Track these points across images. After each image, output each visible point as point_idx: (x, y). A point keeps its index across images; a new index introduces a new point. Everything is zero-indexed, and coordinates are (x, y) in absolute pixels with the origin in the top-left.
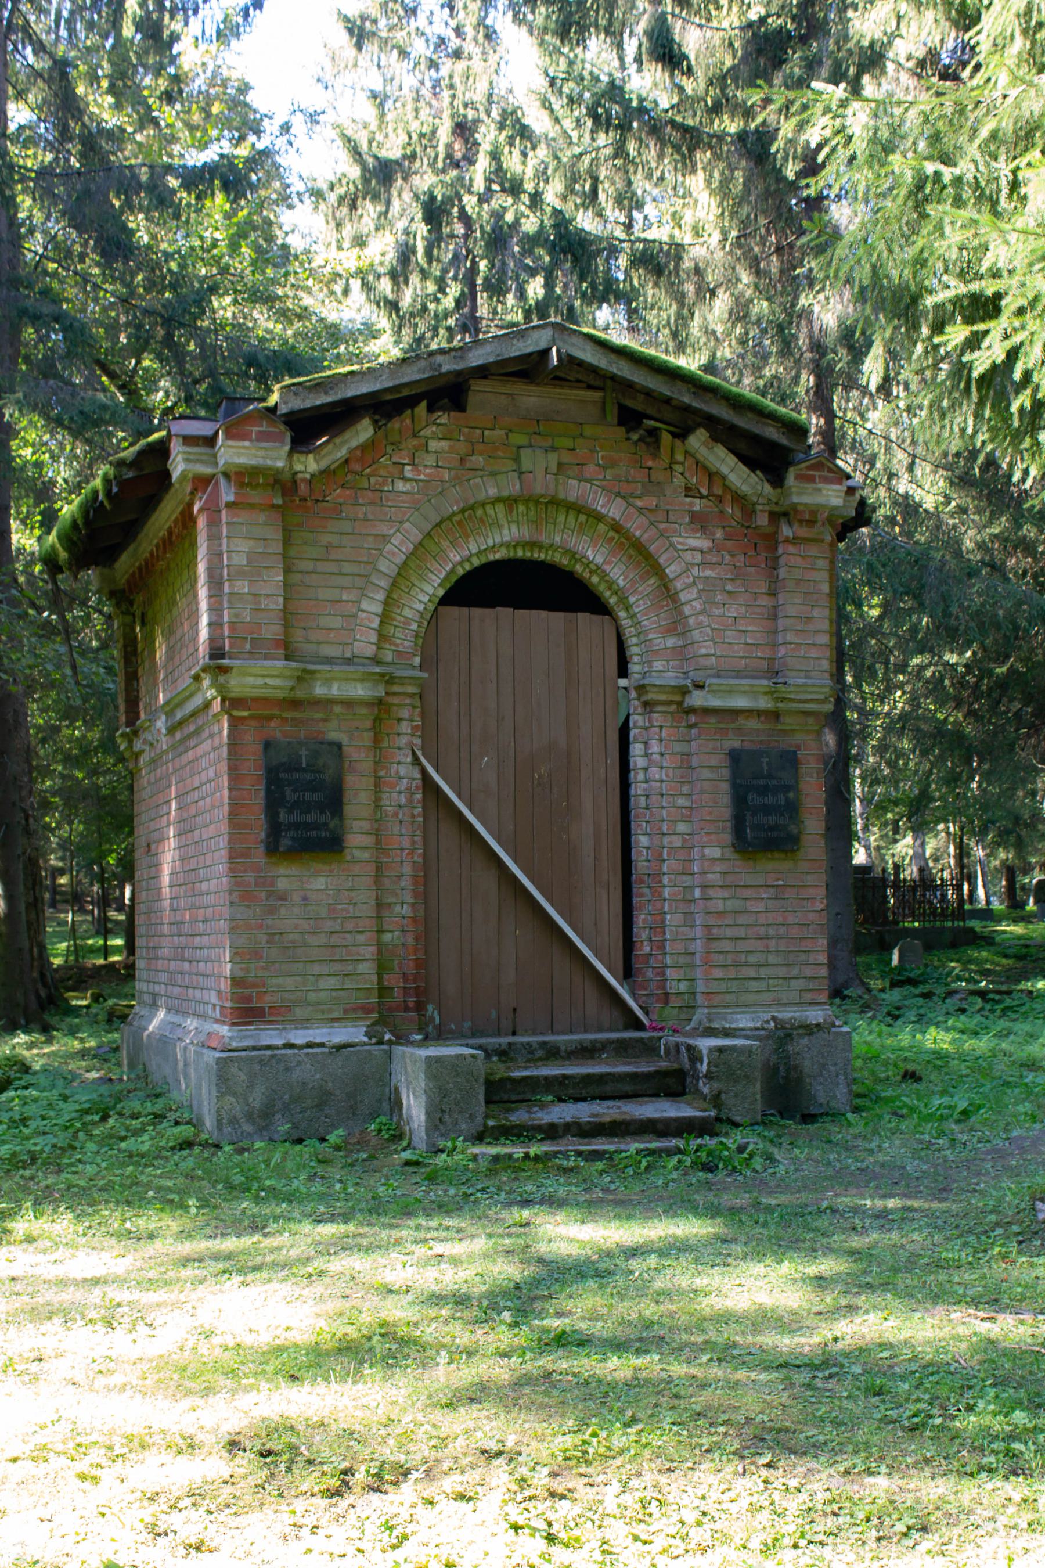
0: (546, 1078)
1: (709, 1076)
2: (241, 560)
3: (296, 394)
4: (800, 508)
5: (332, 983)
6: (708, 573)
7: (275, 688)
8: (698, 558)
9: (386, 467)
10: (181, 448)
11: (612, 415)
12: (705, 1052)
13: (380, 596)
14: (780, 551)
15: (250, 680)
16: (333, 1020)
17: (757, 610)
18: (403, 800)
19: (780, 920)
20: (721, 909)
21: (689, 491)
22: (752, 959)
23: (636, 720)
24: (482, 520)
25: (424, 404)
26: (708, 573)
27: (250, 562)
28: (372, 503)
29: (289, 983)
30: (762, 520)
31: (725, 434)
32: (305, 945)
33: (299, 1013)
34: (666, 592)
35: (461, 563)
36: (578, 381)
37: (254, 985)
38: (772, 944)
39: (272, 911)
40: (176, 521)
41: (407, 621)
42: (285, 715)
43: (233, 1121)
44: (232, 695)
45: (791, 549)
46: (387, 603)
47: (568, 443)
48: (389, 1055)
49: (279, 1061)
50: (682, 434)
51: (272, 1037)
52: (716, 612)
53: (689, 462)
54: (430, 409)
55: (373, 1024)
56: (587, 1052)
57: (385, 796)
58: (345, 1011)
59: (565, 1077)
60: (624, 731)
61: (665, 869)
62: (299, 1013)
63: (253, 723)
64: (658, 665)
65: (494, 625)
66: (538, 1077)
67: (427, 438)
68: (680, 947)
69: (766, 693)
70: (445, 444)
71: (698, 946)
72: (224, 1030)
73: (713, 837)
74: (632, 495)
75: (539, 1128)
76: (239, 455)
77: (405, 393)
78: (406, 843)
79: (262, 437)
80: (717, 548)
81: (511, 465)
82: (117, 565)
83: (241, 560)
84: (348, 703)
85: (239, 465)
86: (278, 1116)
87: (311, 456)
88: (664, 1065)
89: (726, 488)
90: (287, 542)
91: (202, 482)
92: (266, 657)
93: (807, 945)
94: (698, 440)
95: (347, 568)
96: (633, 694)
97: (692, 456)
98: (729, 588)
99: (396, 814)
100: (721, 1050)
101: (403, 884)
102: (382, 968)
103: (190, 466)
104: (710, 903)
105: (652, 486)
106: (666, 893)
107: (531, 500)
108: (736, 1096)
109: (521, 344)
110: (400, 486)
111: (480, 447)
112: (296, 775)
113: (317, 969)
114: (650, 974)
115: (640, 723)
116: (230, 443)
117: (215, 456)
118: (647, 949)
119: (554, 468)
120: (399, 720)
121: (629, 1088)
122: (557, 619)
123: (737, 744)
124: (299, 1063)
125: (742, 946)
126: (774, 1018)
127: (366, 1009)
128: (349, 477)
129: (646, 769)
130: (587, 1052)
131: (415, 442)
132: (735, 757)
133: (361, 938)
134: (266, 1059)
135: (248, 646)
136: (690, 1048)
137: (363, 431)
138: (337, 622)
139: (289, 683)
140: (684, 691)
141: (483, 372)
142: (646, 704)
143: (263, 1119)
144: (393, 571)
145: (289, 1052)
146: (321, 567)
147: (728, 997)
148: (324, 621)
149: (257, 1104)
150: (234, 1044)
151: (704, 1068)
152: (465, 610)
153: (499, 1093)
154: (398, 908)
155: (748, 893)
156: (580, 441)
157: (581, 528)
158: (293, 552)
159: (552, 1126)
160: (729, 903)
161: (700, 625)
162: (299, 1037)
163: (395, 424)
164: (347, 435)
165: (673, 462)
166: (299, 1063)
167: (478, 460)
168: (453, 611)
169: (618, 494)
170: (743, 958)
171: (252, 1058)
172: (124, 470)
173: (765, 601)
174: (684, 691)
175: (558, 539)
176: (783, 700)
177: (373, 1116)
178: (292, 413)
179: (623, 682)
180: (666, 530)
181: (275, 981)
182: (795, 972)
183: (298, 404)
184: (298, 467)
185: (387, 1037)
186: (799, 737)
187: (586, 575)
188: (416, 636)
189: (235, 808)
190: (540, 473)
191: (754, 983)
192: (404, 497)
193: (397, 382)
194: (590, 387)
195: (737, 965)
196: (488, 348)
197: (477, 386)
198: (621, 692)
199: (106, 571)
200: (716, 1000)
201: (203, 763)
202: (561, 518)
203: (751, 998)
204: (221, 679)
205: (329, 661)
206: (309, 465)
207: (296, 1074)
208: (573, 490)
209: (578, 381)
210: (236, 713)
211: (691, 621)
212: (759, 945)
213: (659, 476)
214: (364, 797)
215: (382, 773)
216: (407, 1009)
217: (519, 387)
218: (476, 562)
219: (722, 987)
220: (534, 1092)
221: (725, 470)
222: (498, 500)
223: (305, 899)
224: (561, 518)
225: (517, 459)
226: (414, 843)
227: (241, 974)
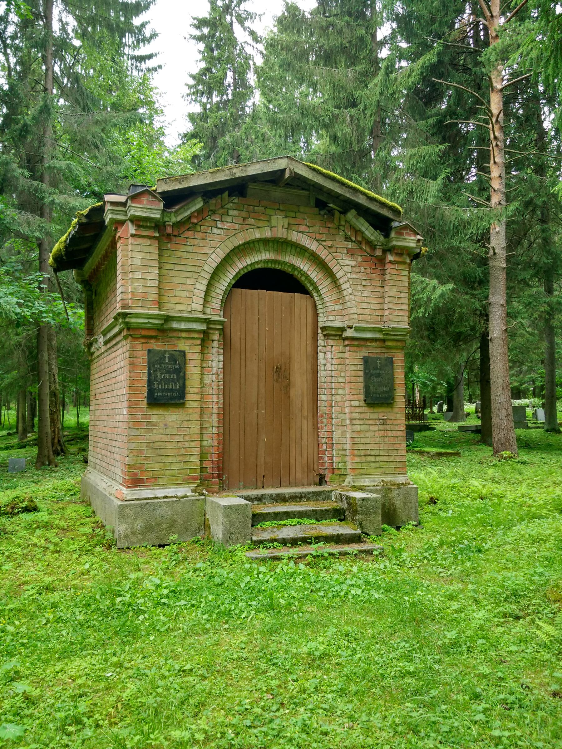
5: (178, 466)
6: (354, 276)
8: (350, 269)
10: (110, 208)
11: (313, 202)
13: (205, 282)
18: (214, 378)
21: (347, 239)
22: (373, 453)
25: (227, 193)
26: (354, 276)
30: (379, 253)
35: (243, 269)
36: (298, 186)
40: (109, 246)
47: (293, 214)
50: (344, 212)
51: (146, 493)
53: (348, 225)
54: (230, 195)
56: (296, 498)
57: (205, 376)
61: (333, 411)
65: (257, 297)
67: (228, 209)
68: (340, 447)
70: (236, 213)
71: (348, 447)
72: (124, 490)
73: (355, 396)
76: (138, 211)
77: (218, 187)
78: (215, 398)
82: (84, 269)
89: (363, 238)
90: (160, 256)
93: (397, 446)
94: (351, 215)
97: (349, 222)
98: (364, 283)
102: (202, 457)
108: (370, 522)
110: (215, 231)
112: (163, 366)
113: (171, 459)
114: (326, 459)
115: (322, 344)
118: (324, 447)
119: (286, 226)
120: (213, 341)
123: (366, 354)
125: (368, 447)
127: (194, 479)
130: (296, 498)
132: (366, 361)
133: (193, 444)
134: (145, 505)
137: (199, 204)
138: (184, 294)
142: (325, 335)
147: (362, 471)
148: (178, 293)
150: (128, 498)
152: (244, 290)
154: (211, 429)
155: (370, 422)
158: (164, 260)
161: (351, 300)
162: (160, 493)
163: (213, 201)
168: (239, 290)
169: (315, 239)
171: (137, 505)
174: (343, 330)
176: (387, 334)
181: (149, 465)
182: (391, 459)
187: (299, 276)
188: (222, 302)
191: (373, 464)
193: (215, 180)
194: (303, 189)
199: (79, 271)
201: (119, 359)
208: (295, 237)
212: (376, 446)
214: (197, 377)
215: (204, 365)
216: (213, 478)
218: (250, 269)
219: (359, 466)
221: (363, 229)
223: (166, 425)
226: (218, 398)
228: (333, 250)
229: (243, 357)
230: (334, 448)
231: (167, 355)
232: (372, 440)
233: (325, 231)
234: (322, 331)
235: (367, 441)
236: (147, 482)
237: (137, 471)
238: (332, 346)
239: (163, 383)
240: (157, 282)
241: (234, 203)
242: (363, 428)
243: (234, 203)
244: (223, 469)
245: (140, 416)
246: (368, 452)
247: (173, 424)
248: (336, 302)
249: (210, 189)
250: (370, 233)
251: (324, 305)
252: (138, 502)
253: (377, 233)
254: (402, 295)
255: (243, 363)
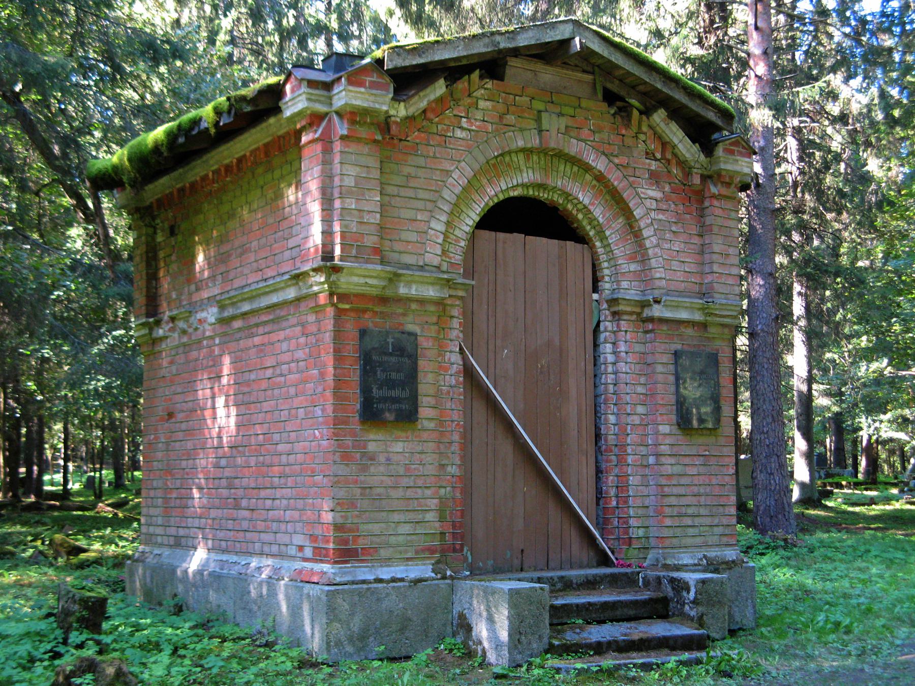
0: (577, 605)
1: (695, 602)
2: (349, 182)
3: (398, 55)
4: (723, 173)
5: (406, 529)
6: (661, 217)
7: (371, 286)
9: (449, 118)
12: (692, 584)
13: (444, 218)
14: (707, 204)
15: (355, 279)
16: (408, 559)
17: (692, 246)
19: (707, 482)
20: (670, 472)
21: (649, 155)
22: (690, 511)
23: (607, 325)
24: (509, 165)
25: (477, 72)
26: (661, 217)
27: (356, 183)
28: (439, 145)
29: (376, 528)
30: (697, 180)
31: (678, 114)
32: (389, 498)
33: (383, 553)
34: (633, 230)
37: (351, 530)
38: (702, 499)
39: (364, 469)
41: (458, 239)
42: (376, 309)
43: (338, 643)
44: (340, 291)
45: (716, 203)
46: (448, 224)
47: (571, 111)
48: (452, 588)
49: (373, 593)
50: (647, 112)
51: (365, 573)
52: (667, 246)
54: (481, 77)
55: (438, 562)
56: (591, 584)
58: (417, 552)
59: (590, 604)
60: (596, 331)
62: (383, 553)
63: (352, 314)
64: (625, 284)
66: (571, 605)
67: (477, 99)
68: (639, 502)
69: (699, 309)
70: (489, 104)
73: (665, 417)
74: (612, 155)
75: (589, 646)
76: (356, 98)
77: (464, 62)
79: (374, 85)
80: (667, 199)
81: (533, 124)
83: (349, 182)
84: (422, 301)
85: (353, 106)
86: (372, 639)
87: (402, 104)
88: (645, 595)
89: (675, 155)
91: (316, 119)
92: (368, 261)
94: (659, 116)
95: (422, 194)
96: (605, 306)
98: (674, 229)
99: (448, 392)
100: (703, 582)
101: (453, 448)
103: (311, 105)
104: (662, 468)
105: (625, 149)
106: (630, 460)
107: (543, 151)
109: (552, 33)
110: (459, 133)
111: (512, 109)
113: (396, 517)
115: (610, 328)
116: (351, 88)
117: (330, 98)
119: (563, 130)
120: (452, 317)
121: (632, 613)
122: (553, 245)
123: (679, 347)
124: (388, 595)
125: (684, 501)
126: (705, 556)
127: (431, 550)
128: (424, 123)
129: (614, 364)
131: (469, 100)
133: (428, 492)
134: (364, 591)
135: (354, 252)
136: (672, 580)
137: (439, 88)
138: (413, 237)
139: (383, 283)
140: (644, 304)
141: (516, 52)
142: (614, 314)
143: (361, 640)
144: (453, 199)
145: (380, 585)
146: (403, 192)
147: (674, 541)
148: (405, 236)
149: (356, 629)
150: (338, 579)
151: (692, 595)
152: (493, 233)
153: (560, 617)
155: (687, 461)
156: (578, 110)
157: (575, 177)
159: (599, 644)
160: (675, 468)
161: (656, 256)
162: (385, 573)
164: (428, 90)
165: (640, 131)
166: (388, 595)
167: (511, 118)
169: (603, 153)
170: (683, 510)
171: (352, 592)
172: (244, 105)
173: (696, 240)
174: (644, 304)
175: (559, 183)
177: (441, 638)
178: (396, 69)
179: (595, 296)
180: (634, 182)
181: (365, 527)
182: (716, 521)
183: (400, 62)
184: (392, 112)
185: (449, 573)
186: (718, 343)
187: (574, 212)
189: (339, 382)
190: (554, 132)
192: (460, 142)
193: (470, 53)
194: (584, 71)
195: (680, 516)
196: (530, 33)
197: (513, 62)
198: (595, 303)
200: (667, 543)
202: (562, 168)
203: (689, 541)
204: (333, 277)
205: (407, 267)
206: (401, 111)
207: (385, 604)
208: (574, 147)
209: (576, 66)
210: (341, 306)
211: (650, 252)
213: (629, 141)
217: (539, 66)
220: (569, 617)
221: (676, 141)
222: (523, 150)
223: (388, 459)
224: (562, 168)
225: (538, 120)
227: (341, 521)
228: (630, 172)
229: (491, 347)
230: (631, 503)
231: (390, 340)
232: (688, 490)
233: (617, 140)
234: (609, 306)
235: (681, 490)
236: (363, 554)
237: (350, 536)
238: (626, 331)
239: (385, 388)
240: (378, 216)
241: (485, 89)
242: (677, 469)
243: (485, 89)
244: (462, 537)
245: (350, 444)
246: (683, 510)
247: (400, 457)
248: (632, 258)
249: (452, 64)
250: (687, 148)
251: (612, 263)
252: (355, 586)
253: (695, 148)
254: (731, 251)
255: (491, 355)
